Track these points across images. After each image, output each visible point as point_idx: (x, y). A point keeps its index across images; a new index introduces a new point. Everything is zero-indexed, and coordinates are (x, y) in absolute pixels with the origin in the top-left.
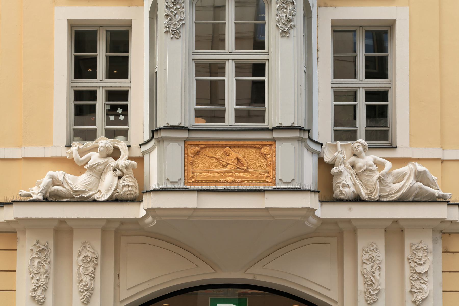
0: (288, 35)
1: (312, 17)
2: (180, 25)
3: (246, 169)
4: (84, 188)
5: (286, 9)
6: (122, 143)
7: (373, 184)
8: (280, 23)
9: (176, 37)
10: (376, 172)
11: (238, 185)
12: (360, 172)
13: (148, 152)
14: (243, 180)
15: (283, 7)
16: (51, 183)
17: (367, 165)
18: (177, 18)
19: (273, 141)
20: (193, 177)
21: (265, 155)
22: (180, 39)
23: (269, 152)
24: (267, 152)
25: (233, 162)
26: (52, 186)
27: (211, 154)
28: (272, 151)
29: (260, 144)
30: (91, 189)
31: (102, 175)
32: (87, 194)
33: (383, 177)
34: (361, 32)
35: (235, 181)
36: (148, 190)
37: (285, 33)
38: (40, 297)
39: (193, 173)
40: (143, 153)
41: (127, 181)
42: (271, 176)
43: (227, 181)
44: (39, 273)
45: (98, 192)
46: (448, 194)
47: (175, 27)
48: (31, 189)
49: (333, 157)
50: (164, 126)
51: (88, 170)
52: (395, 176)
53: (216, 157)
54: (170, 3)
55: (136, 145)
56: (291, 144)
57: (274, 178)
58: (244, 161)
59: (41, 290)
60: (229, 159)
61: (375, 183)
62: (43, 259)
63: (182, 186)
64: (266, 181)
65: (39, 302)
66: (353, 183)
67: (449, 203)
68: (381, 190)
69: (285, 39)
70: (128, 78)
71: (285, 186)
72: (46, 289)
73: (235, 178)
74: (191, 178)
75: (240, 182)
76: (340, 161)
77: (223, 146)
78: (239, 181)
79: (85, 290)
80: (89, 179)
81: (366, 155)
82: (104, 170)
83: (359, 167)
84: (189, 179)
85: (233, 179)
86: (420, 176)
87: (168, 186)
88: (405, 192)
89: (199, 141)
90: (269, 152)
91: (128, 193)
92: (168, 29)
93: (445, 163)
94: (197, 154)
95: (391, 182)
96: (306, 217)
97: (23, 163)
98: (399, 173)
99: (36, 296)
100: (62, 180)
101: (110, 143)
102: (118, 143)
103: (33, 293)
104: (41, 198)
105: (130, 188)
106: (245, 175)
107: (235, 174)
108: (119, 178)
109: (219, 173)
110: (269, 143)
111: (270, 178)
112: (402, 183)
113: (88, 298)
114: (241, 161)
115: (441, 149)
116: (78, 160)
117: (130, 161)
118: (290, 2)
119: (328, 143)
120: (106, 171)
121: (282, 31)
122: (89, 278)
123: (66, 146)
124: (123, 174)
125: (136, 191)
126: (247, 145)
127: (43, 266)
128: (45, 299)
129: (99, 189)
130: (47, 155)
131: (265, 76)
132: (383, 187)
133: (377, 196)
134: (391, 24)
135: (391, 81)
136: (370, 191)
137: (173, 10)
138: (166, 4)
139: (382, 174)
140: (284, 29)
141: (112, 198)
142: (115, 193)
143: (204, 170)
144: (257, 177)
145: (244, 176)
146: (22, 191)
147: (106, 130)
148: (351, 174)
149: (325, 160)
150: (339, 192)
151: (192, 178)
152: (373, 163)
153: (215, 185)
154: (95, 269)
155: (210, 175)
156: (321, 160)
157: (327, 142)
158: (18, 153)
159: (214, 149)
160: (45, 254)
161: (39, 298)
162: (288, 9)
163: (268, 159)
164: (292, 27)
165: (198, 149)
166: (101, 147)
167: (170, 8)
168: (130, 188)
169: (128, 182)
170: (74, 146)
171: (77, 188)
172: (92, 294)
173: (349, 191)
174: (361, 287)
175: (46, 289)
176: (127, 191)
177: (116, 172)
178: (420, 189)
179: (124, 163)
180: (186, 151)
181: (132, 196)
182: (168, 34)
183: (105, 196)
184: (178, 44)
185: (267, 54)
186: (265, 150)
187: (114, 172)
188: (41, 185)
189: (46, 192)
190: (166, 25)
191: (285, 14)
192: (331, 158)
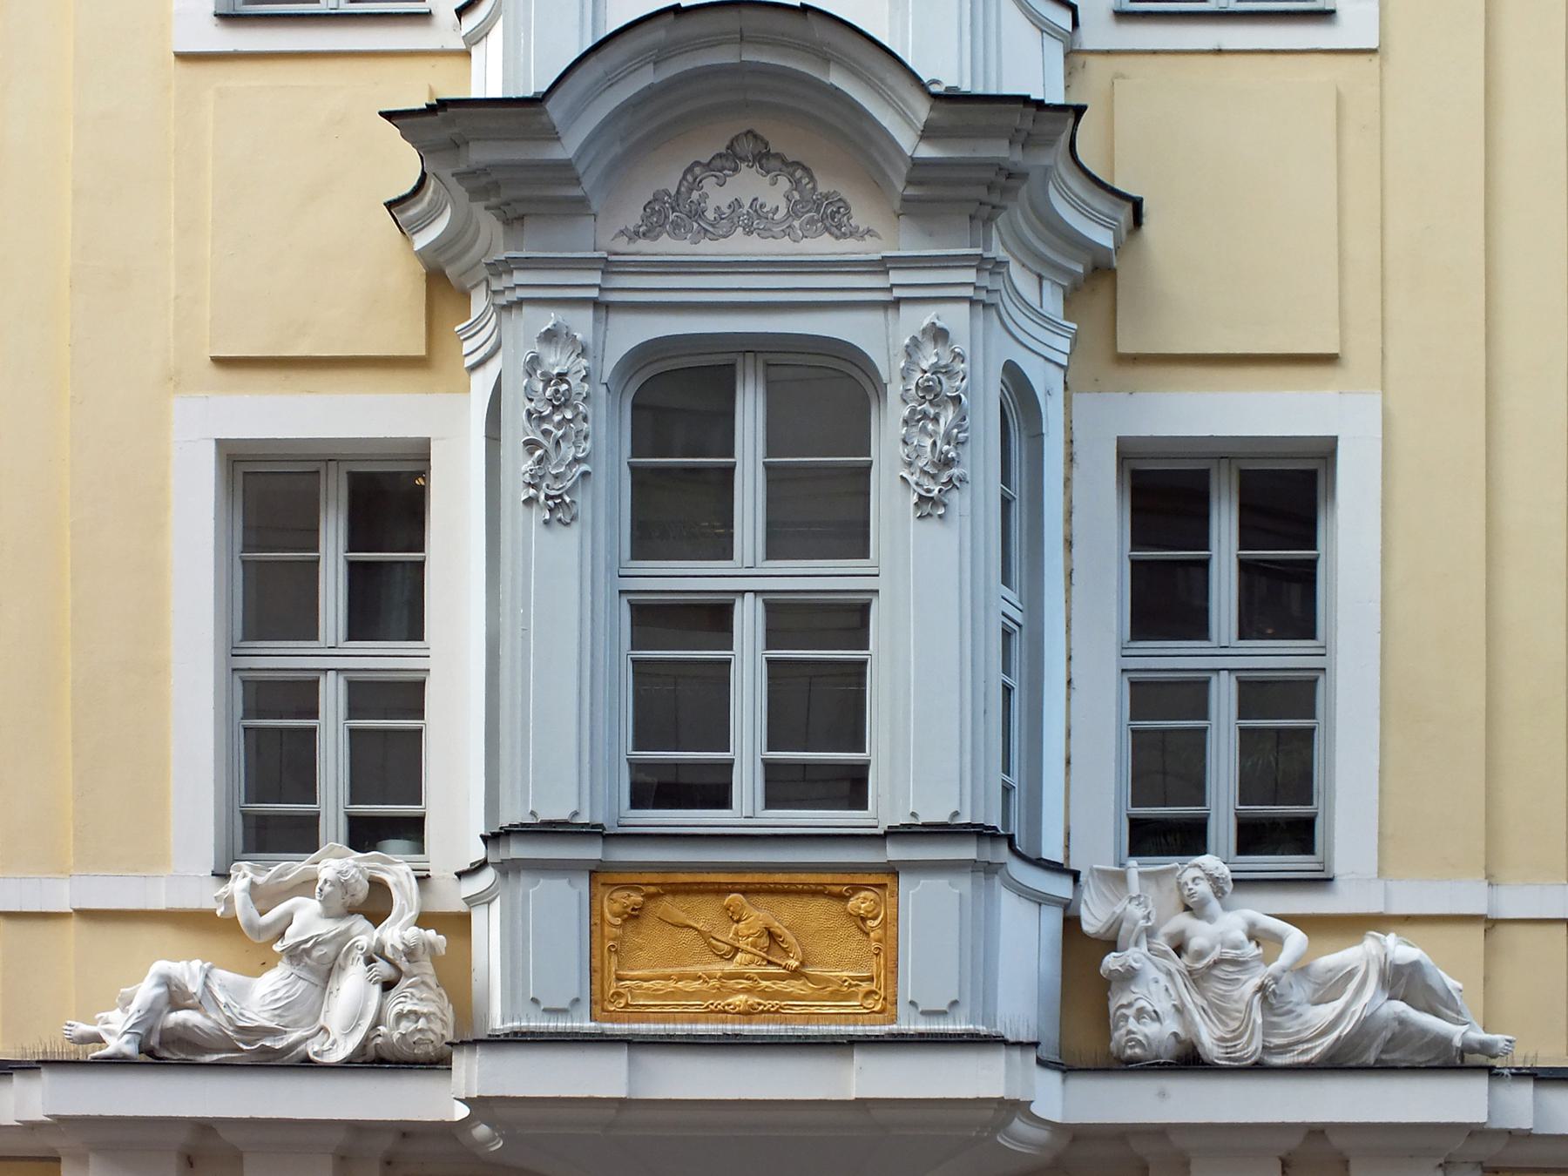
0: (941, 511)
1: (1043, 434)
2: (575, 478)
3: (797, 967)
5: (936, 419)
6: (400, 867)
7: (1242, 1006)
10: (1253, 967)
11: (775, 1022)
12: (1199, 969)
14: (785, 1003)
15: (925, 415)
16: (164, 1000)
17: (1222, 944)
18: (562, 453)
21: (864, 919)
22: (576, 527)
23: (874, 910)
24: (869, 909)
25: (754, 945)
26: (168, 1009)
27: (682, 917)
29: (845, 885)
30: (296, 1024)
32: (282, 1039)
33: (1274, 986)
34: (1224, 479)
35: (762, 1007)
36: (464, 1039)
39: (620, 979)
40: (471, 901)
41: (411, 999)
42: (882, 992)
43: (732, 1007)
45: (320, 1031)
46: (1499, 1039)
48: (101, 1017)
49: (1112, 916)
50: (520, 821)
51: (284, 959)
52: (1318, 981)
53: (695, 925)
54: (541, 400)
55: (447, 874)
56: (950, 884)
58: (791, 939)
60: (740, 934)
61: (1249, 1006)
64: (865, 1008)
66: (1174, 1006)
67: (1492, 1072)
68: (1269, 1027)
69: (932, 526)
71: (923, 1026)
74: (612, 996)
75: (777, 1012)
76: (1133, 930)
77: (720, 890)
78: (773, 1007)
81: (1225, 908)
82: (336, 959)
83: (1196, 951)
85: (753, 1000)
87: (532, 1024)
88: (1347, 1034)
89: (640, 873)
90: (875, 912)
92: (535, 491)
93: (1503, 932)
94: (633, 916)
95: (1305, 1000)
96: (1002, 1125)
97: (73, 925)
98: (1330, 970)
100: (199, 994)
101: (355, 869)
102: (385, 867)
104: (130, 1049)
105: (422, 1023)
106: (794, 986)
107: (759, 983)
108: (388, 986)
109: (706, 982)
110: (873, 879)
111: (877, 998)
112: (1338, 1005)
114: (782, 942)
115: (1486, 883)
116: (251, 926)
117: (422, 930)
118: (947, 396)
119: (1098, 870)
120: (342, 964)
123: (213, 875)
124: (400, 972)
125: (442, 1029)
129: (322, 1022)
130: (161, 903)
131: (868, 649)
132: (1275, 1019)
133: (1252, 1048)
134: (1326, 450)
135: (1324, 647)
136: (1233, 1031)
137: (549, 427)
139: (1269, 975)
140: (929, 491)
143: (657, 969)
144: (835, 995)
146: (72, 1023)
148: (1169, 974)
149: (1086, 927)
150: (1127, 1035)
151: (615, 997)
152: (1243, 937)
153: (692, 1022)
156: (1071, 923)
157: (1095, 866)
158: (62, 897)
159: (690, 899)
162: (942, 421)
163: (872, 934)
164: (954, 485)
165: (637, 898)
166: (326, 881)
167: (542, 419)
168: (422, 1023)
170: (237, 876)
171: (249, 1018)
173: (1158, 1032)
176: (413, 1033)
178: (1399, 1024)
180: (597, 907)
182: (535, 508)
183: (342, 1047)
184: (568, 541)
186: (861, 902)
187: (367, 969)
188: (133, 1007)
189: (150, 1031)
190: (527, 478)
191: (931, 436)
192: (1105, 920)
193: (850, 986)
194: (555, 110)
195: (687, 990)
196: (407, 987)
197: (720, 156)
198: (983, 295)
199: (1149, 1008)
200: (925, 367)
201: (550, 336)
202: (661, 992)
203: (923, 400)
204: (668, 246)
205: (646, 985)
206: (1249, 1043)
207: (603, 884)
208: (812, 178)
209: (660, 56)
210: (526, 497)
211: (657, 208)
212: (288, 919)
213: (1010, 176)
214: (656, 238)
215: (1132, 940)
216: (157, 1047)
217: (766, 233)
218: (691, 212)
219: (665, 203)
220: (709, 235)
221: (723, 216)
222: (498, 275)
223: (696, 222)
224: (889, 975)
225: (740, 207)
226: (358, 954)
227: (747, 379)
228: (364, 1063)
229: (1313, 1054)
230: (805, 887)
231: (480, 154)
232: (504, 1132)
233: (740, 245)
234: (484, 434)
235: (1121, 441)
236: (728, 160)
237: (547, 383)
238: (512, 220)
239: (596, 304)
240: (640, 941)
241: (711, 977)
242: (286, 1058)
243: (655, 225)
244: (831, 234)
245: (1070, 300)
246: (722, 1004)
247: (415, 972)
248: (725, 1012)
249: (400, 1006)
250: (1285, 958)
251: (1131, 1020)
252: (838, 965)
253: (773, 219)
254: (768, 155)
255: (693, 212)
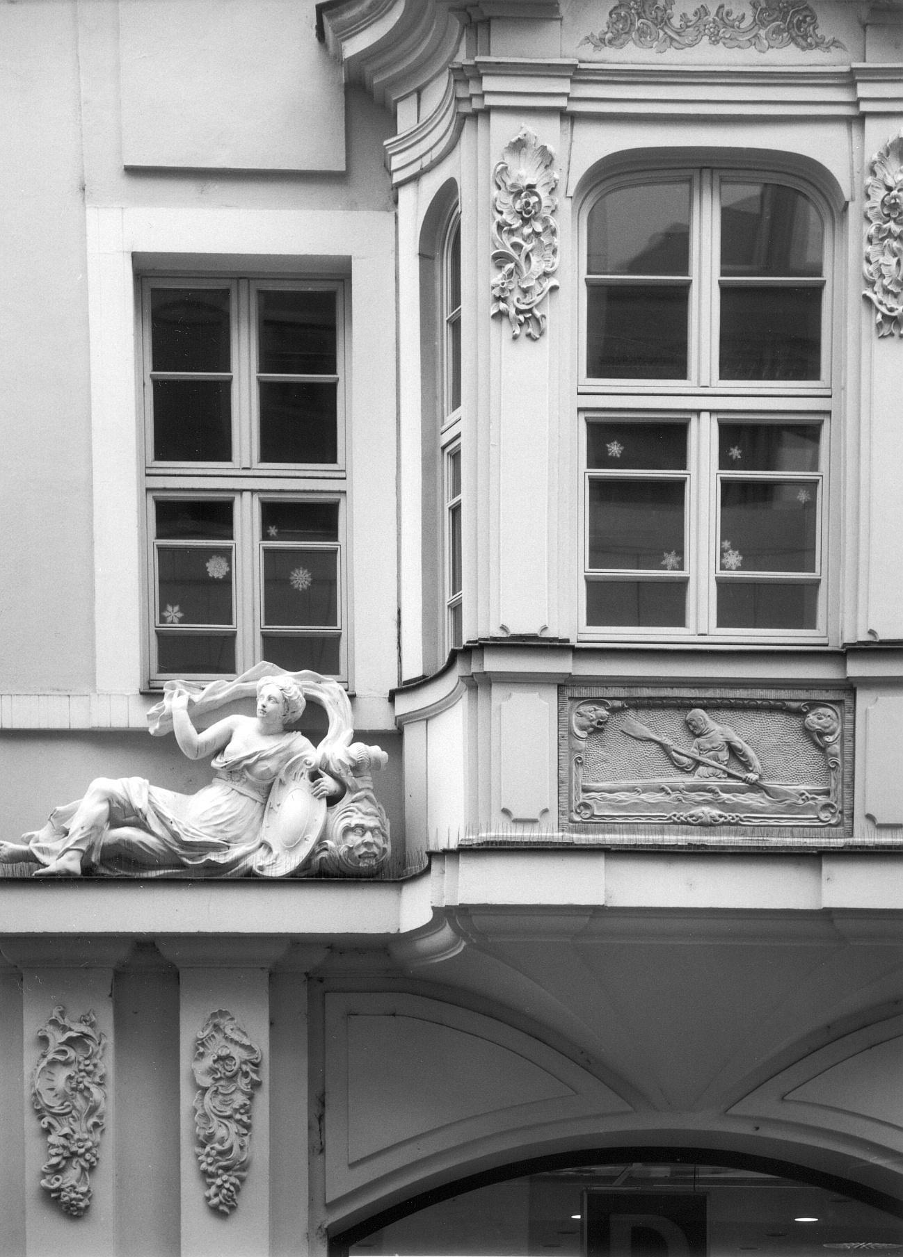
3: (757, 780)
4: (214, 835)
8: (876, 289)
9: (529, 335)
11: (736, 834)
13: (421, 718)
14: (745, 815)
16: (106, 816)
18: (532, 266)
19: (845, 690)
20: (586, 806)
21: (821, 734)
22: (545, 342)
24: (826, 725)
28: (843, 723)
31: (270, 790)
32: (225, 854)
35: (722, 819)
38: (75, 1192)
39: (586, 790)
41: (357, 813)
43: (694, 818)
44: (70, 1112)
47: (528, 300)
51: (223, 775)
53: (658, 739)
57: (846, 812)
58: (750, 752)
59: (79, 1169)
62: (82, 1067)
63: (548, 832)
65: (72, 1209)
70: (334, 461)
72: (95, 1164)
73: (722, 810)
75: (736, 824)
78: (733, 819)
79: (220, 1168)
80: (229, 804)
84: (572, 811)
85: (715, 812)
89: (606, 687)
91: (362, 853)
94: (597, 730)
99: (63, 1190)
103: (53, 1180)
105: (368, 837)
107: (719, 796)
108: (332, 800)
110: (830, 696)
113: (233, 1195)
116: (189, 744)
117: (367, 746)
120: (284, 779)
121: (882, 318)
122: (234, 1127)
124: (344, 788)
126: (759, 702)
127: (81, 1091)
128: (89, 1199)
130: (79, 723)
138: (499, 218)
140: (891, 310)
141: (309, 868)
142: (319, 852)
144: (792, 808)
145: (749, 805)
147: (266, 638)
154: (251, 1097)
155: (638, 799)
160: (91, 1051)
161: (73, 1195)
165: (603, 712)
169: (360, 815)
172: (242, 1180)
175: (95, 1164)
176: (359, 846)
177: (323, 781)
179: (346, 752)
181: (373, 862)
182: (505, 321)
185: (827, 392)
189: (91, 848)
190: (496, 292)
191: (895, 255)
195: (650, 801)
196: (353, 802)
200: (890, 183)
201: (518, 146)
202: (624, 804)
203: (888, 218)
204: (632, 55)
207: (570, 698)
210: (495, 311)
211: (623, 14)
214: (622, 46)
216: (98, 864)
217: (732, 43)
218: (656, 18)
219: (631, 9)
220: (675, 44)
221: (689, 24)
222: (466, 81)
223: (662, 29)
224: (845, 789)
225: (706, 14)
227: (704, 195)
228: (308, 876)
230: (764, 703)
232: (475, 941)
233: (706, 55)
234: (417, 251)
240: (604, 754)
242: (229, 873)
243: (620, 31)
244: (797, 44)
246: (685, 815)
249: (347, 821)
253: (739, 28)
255: (659, 19)
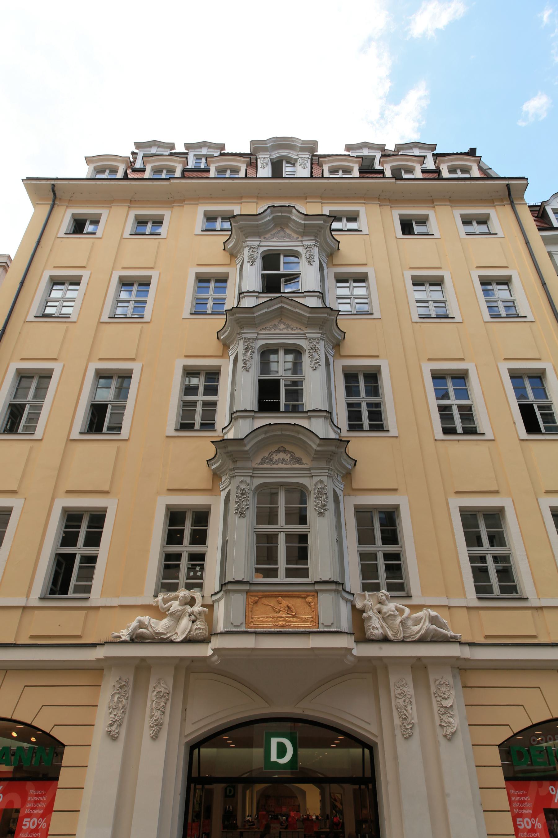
5: (321, 497)
7: (397, 626)
11: (289, 628)
21: (310, 603)
25: (284, 609)
27: (267, 603)
30: (170, 632)
37: (321, 514)
42: (315, 621)
58: (293, 608)
66: (381, 626)
69: (321, 518)
71: (326, 629)
75: (290, 626)
77: (277, 596)
81: (389, 603)
86: (433, 620)
93: (451, 609)
94: (256, 602)
104: (128, 639)
105: (201, 631)
106: (294, 619)
108: (193, 622)
112: (420, 625)
115: (447, 598)
116: (162, 607)
125: (206, 633)
129: (176, 631)
132: (405, 630)
144: (304, 622)
149: (357, 607)
156: (354, 607)
167: (239, 497)
168: (201, 631)
173: (378, 632)
174: (397, 721)
182: (237, 514)
184: (244, 521)
186: (309, 599)
188: (130, 628)
189: (133, 634)
190: (236, 508)
193: (307, 619)
194: (246, 441)
197: (276, 450)
198: (329, 475)
199: (375, 626)
200: (319, 487)
201: (242, 482)
204: (265, 466)
205: (258, 619)
206: (400, 635)
208: (294, 455)
209: (266, 433)
212: (171, 606)
213: (334, 454)
214: (263, 465)
215: (369, 610)
226: (188, 614)
229: (416, 638)
231: (230, 448)
233: (280, 466)
235: (355, 505)
236: (278, 451)
237: (241, 491)
238: (234, 461)
239: (251, 476)
241: (274, 617)
245: (342, 477)
247: (201, 618)
248: (278, 626)
249: (196, 627)
250: (406, 614)
251: (371, 629)
252: (305, 614)
254: (286, 450)
